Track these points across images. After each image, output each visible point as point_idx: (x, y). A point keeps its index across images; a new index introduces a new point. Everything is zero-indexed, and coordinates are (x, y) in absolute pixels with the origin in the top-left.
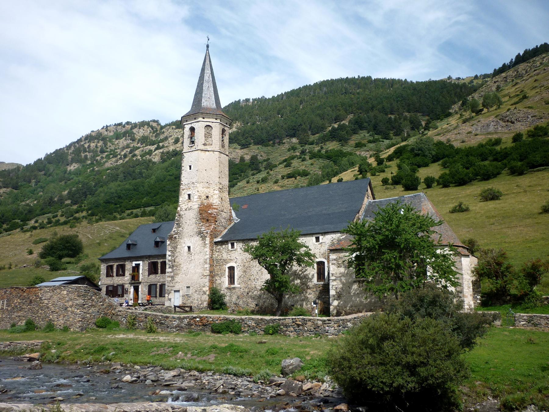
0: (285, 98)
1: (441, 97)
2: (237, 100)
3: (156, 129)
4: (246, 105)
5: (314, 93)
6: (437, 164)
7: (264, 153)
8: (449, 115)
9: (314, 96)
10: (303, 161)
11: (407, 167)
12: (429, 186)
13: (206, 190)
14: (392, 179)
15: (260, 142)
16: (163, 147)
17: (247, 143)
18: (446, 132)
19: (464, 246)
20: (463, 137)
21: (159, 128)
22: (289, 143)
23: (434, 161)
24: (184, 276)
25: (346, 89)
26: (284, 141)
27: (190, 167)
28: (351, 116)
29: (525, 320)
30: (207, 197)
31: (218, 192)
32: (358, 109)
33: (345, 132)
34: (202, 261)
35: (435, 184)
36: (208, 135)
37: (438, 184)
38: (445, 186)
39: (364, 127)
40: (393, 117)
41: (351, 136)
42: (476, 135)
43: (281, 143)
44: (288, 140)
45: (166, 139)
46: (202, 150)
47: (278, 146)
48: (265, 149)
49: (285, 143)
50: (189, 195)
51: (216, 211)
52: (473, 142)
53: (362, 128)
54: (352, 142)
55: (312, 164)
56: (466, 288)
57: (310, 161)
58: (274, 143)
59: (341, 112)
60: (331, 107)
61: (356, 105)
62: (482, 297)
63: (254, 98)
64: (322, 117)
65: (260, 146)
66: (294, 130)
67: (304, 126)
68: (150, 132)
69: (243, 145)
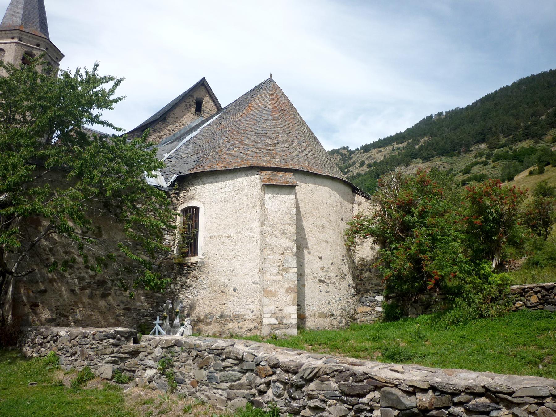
0: (479, 104)
2: (429, 115)
3: (345, 155)
4: (439, 119)
7: (448, 163)
10: (485, 165)
15: (444, 153)
16: (348, 171)
17: (429, 156)
21: (348, 155)
22: (477, 149)
26: (471, 149)
33: (539, 127)
38: (105, 77)
41: (547, 131)
43: (467, 151)
44: (476, 147)
45: (354, 163)
47: (464, 155)
48: (449, 160)
49: (472, 151)
55: (494, 167)
57: (493, 164)
58: (460, 152)
62: (387, 298)
63: (447, 110)
64: (516, 116)
65: (443, 158)
66: (482, 134)
67: (494, 129)
68: (340, 160)
69: (425, 159)
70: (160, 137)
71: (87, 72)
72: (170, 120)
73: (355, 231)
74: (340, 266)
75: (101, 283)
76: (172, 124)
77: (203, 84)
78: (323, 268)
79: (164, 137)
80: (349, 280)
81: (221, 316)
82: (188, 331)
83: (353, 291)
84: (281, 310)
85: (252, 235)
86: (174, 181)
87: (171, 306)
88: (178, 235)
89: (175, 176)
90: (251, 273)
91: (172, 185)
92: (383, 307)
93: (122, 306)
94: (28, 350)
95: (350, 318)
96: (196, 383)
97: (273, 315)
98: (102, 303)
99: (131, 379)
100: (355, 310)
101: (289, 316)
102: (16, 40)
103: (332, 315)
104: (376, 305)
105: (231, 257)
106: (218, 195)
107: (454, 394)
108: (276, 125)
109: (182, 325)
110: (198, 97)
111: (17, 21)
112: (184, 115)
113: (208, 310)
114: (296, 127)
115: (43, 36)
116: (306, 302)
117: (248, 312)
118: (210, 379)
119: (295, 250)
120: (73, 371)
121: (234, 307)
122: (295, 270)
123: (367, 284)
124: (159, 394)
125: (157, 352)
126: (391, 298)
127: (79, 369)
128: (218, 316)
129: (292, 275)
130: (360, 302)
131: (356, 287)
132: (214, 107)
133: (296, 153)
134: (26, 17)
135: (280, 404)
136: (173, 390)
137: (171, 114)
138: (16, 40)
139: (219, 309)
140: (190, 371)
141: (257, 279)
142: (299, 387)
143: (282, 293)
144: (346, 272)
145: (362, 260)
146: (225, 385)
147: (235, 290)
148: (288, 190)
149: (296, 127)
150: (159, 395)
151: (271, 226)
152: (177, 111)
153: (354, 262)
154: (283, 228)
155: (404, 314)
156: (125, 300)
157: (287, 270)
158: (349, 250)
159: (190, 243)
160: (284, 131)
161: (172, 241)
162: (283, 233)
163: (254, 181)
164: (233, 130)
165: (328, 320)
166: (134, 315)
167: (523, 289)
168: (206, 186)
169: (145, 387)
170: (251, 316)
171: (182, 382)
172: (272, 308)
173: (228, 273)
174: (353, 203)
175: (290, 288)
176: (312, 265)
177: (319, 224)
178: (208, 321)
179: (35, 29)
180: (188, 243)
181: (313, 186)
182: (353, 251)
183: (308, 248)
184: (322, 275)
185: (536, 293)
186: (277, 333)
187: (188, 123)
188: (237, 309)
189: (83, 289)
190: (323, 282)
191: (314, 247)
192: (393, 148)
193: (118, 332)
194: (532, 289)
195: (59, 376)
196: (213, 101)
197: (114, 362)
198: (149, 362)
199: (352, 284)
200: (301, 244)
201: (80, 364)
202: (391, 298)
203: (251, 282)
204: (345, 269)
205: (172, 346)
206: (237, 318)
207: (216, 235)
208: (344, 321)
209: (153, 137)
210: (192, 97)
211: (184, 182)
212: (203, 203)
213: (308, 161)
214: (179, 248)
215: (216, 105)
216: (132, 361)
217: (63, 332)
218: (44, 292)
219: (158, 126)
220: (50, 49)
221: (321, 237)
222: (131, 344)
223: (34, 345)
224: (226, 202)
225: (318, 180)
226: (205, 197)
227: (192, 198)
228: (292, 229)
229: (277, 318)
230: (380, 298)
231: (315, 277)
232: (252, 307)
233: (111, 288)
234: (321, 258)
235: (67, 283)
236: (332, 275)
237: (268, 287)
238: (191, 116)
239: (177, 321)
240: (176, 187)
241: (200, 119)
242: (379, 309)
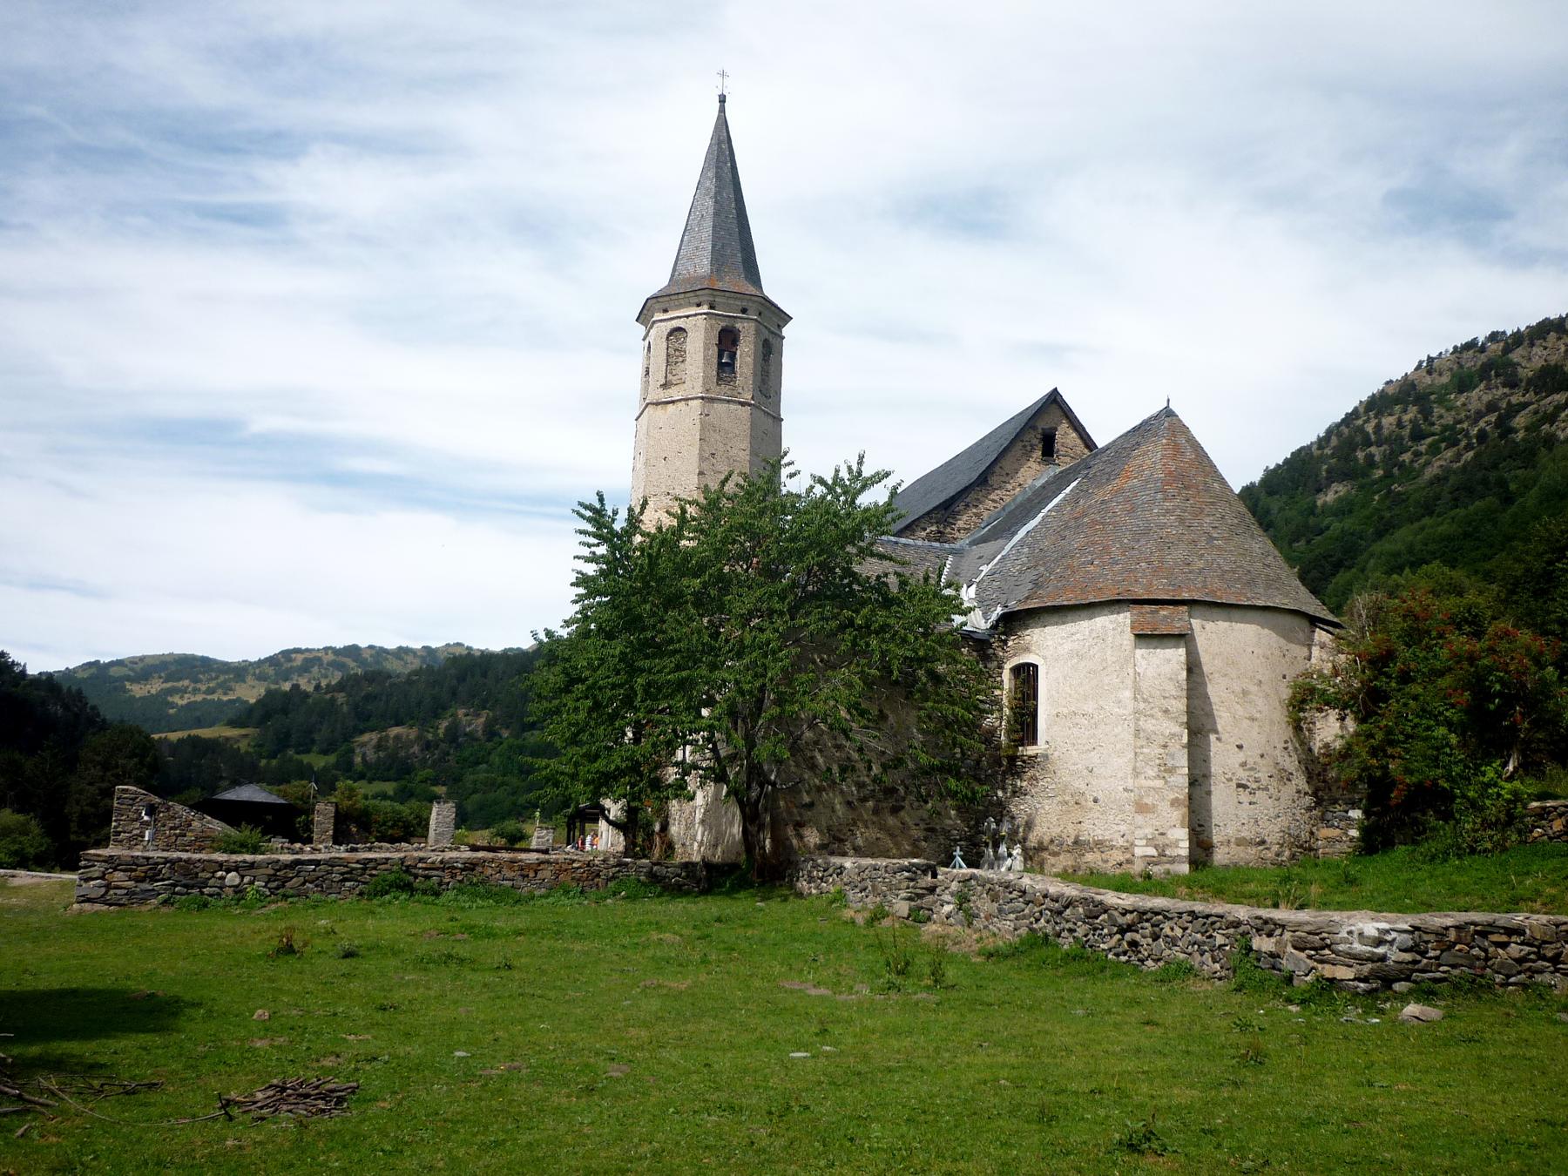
46: (657, 404)
70: (978, 515)
71: (850, 468)
72: (993, 480)
73: (1304, 700)
74: (1280, 760)
75: (890, 791)
76: (1000, 488)
77: (1054, 401)
78: (1244, 764)
79: (986, 515)
80: (1300, 781)
81: (1076, 842)
82: (1018, 864)
83: (1308, 801)
85: (1122, 711)
86: (997, 621)
87: (994, 826)
88: (1007, 711)
89: (999, 610)
90: (1120, 775)
91: (994, 627)
92: (1359, 829)
93: (922, 826)
94: (802, 884)
95: (1301, 846)
96: (989, 917)
97: (1150, 842)
98: (891, 821)
99: (929, 919)
100: (1312, 833)
101: (1176, 844)
102: (705, 309)
103: (1263, 842)
104: (1349, 826)
106: (1068, 646)
107: (1144, 913)
108: (1168, 511)
109: (1010, 855)
110: (1045, 426)
111: (703, 266)
112: (1021, 466)
113: (1055, 831)
114: (1207, 510)
115: (751, 290)
116: (1214, 821)
117: (1117, 836)
118: (1000, 911)
119: (1185, 740)
120: (865, 909)
121: (1093, 829)
122: (1186, 770)
123: (1334, 789)
124: (957, 930)
125: (954, 886)
126: (1374, 814)
127: (871, 906)
128: (1070, 842)
129: (1181, 779)
130: (1322, 819)
131: (1315, 794)
132: (1079, 441)
133: (1201, 564)
134: (718, 258)
135: (1049, 930)
136: (970, 924)
137: (997, 469)
138: (705, 309)
139: (1071, 832)
140: (984, 905)
141: (1130, 783)
142: (1060, 913)
143: (1164, 807)
144: (1292, 769)
145: (1327, 746)
146: (1012, 916)
147: (1096, 801)
148: (1173, 642)
149: (1207, 510)
150: (957, 930)
152: (1007, 464)
153: (1310, 750)
154: (1166, 704)
155: (1388, 844)
156: (925, 816)
157: (1171, 770)
158: (1298, 729)
159: (1025, 724)
160: (1181, 520)
161: (999, 722)
162: (1166, 711)
163: (1116, 626)
164: (1094, 522)
165: (1253, 851)
166: (942, 839)
167: (1544, 808)
168: (1048, 629)
169: (942, 923)
170: (1121, 842)
171: (977, 916)
172: (1149, 831)
173: (1085, 772)
174: (1309, 646)
175: (1177, 799)
176: (1223, 758)
177: (1238, 689)
178: (1057, 849)
179: (735, 282)
180: (1022, 724)
181: (1226, 624)
182: (1309, 730)
183: (1216, 732)
184: (1242, 775)
185: (1560, 815)
186: (1156, 870)
187: (1030, 482)
189: (864, 800)
190: (1245, 787)
191: (1229, 728)
193: (913, 865)
194: (1555, 808)
195: (848, 914)
196: (1076, 430)
197: (910, 899)
198: (947, 897)
199: (1306, 788)
200: (1199, 726)
201: (872, 901)
202: (1374, 814)
204: (1291, 763)
206: (1099, 845)
207: (1065, 711)
208: (1287, 853)
209: (965, 518)
210: (1034, 428)
211: (1012, 622)
212: (1045, 658)
213: (1222, 578)
214: (1009, 732)
215: (1081, 438)
216: (931, 898)
217: (848, 863)
218: (811, 805)
219: (973, 495)
220: (766, 312)
221: (1240, 711)
222: (929, 878)
223: (811, 880)
224: (1081, 657)
225: (1237, 614)
226: (1048, 648)
227: (1027, 650)
228: (1180, 706)
229: (1156, 847)
230: (1356, 814)
231: (1230, 780)
232: (1123, 828)
233: (904, 799)
234: (1240, 747)
235: (842, 792)
236: (1263, 776)
238: (1035, 466)
239: (1003, 849)
240: (1001, 629)
241: (1053, 471)
242: (1354, 833)
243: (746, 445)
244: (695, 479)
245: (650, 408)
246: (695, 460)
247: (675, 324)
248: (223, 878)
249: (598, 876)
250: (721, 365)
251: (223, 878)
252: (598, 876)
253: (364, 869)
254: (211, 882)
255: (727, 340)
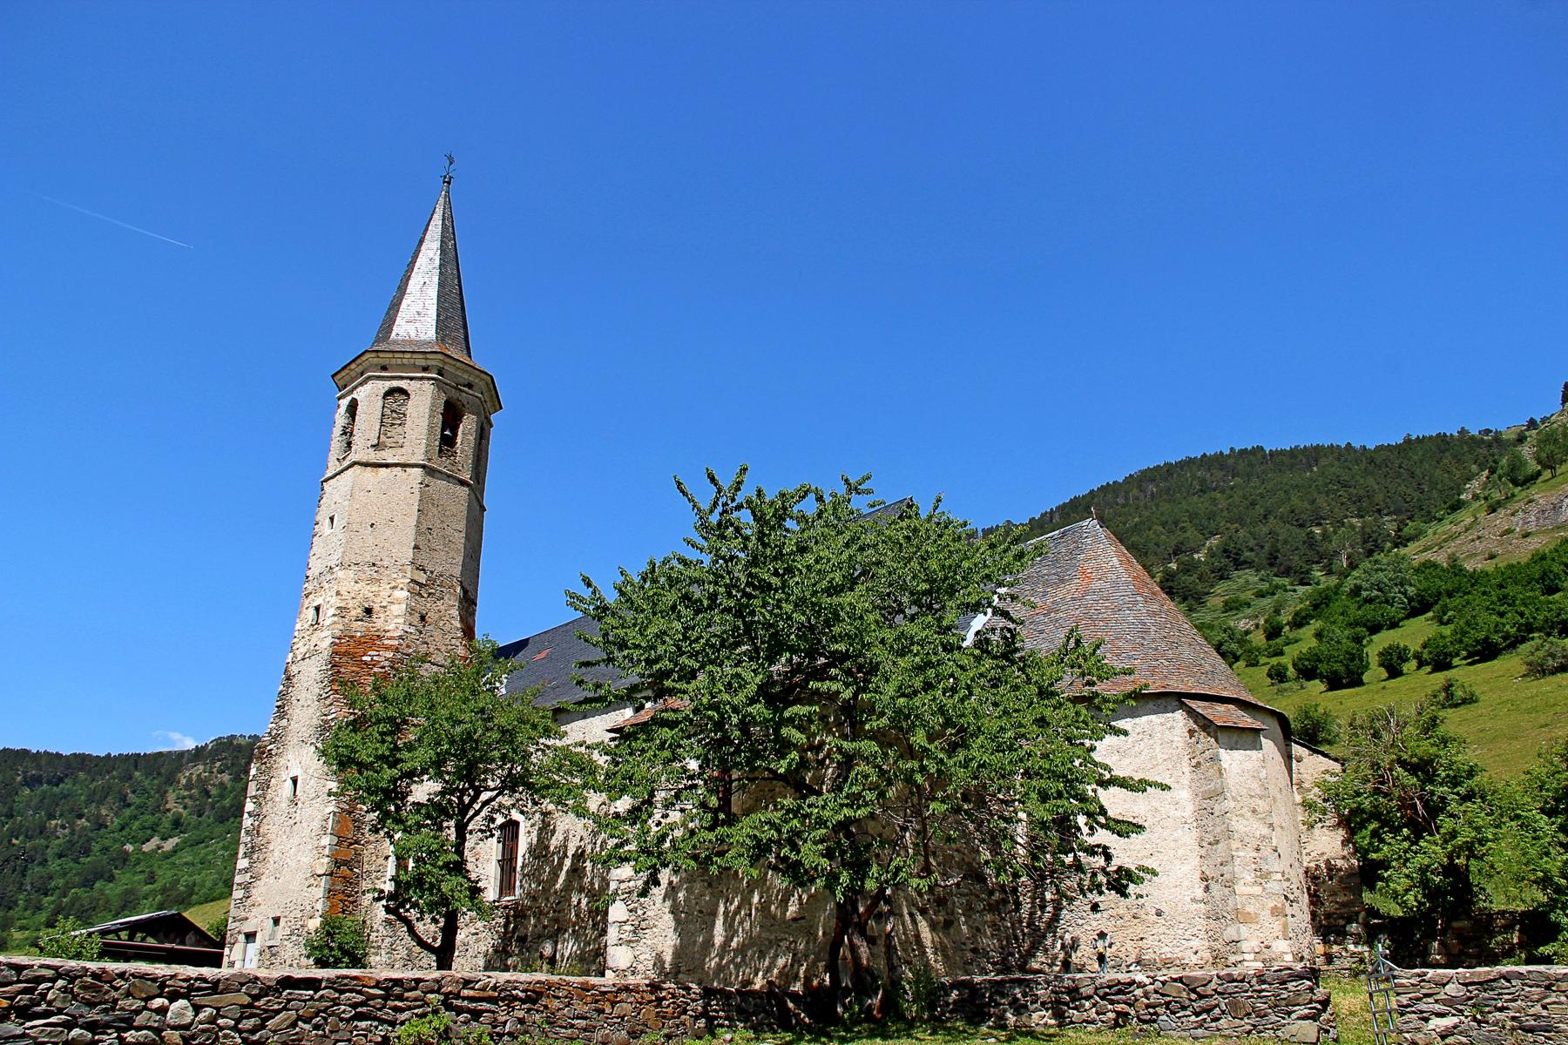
1: (1438, 472)
5: (1127, 498)
6: (1422, 618)
8: (1457, 506)
9: (1124, 506)
11: (1342, 634)
12: (1394, 672)
13: (366, 590)
14: (1294, 665)
18: (1445, 541)
19: (1245, 696)
20: (1491, 543)
23: (1414, 613)
24: (272, 880)
25: (1203, 481)
27: (332, 519)
28: (1214, 541)
29: (1450, 1001)
30: (369, 611)
31: (405, 594)
32: (1230, 521)
34: (316, 825)
35: (1413, 664)
36: (393, 416)
37: (1420, 665)
39: (1245, 562)
40: (1318, 531)
41: (1212, 586)
42: (1526, 536)
46: (366, 465)
50: (317, 609)
51: (390, 655)
52: (1522, 553)
53: (1239, 564)
54: (1215, 601)
56: (1249, 878)
59: (1189, 534)
60: (1164, 524)
61: (1225, 513)
84: (1268, 947)
85: (1178, 814)
90: (1186, 883)
105: (1145, 853)
117: (1189, 953)
134: (441, 325)
147: (1159, 913)
151: (1234, 799)
188: (1166, 949)
192: (1448, 688)
203: (1188, 899)
205: (1494, 980)
232: (1195, 943)
237: (1244, 906)
243: (462, 526)
244: (410, 554)
245: (357, 467)
246: (412, 532)
247: (395, 384)
248: (162, 1011)
249: (685, 1012)
250: (443, 437)
251: (162, 1011)
252: (685, 1012)
253: (386, 998)
254: (139, 1020)
255: (451, 416)
